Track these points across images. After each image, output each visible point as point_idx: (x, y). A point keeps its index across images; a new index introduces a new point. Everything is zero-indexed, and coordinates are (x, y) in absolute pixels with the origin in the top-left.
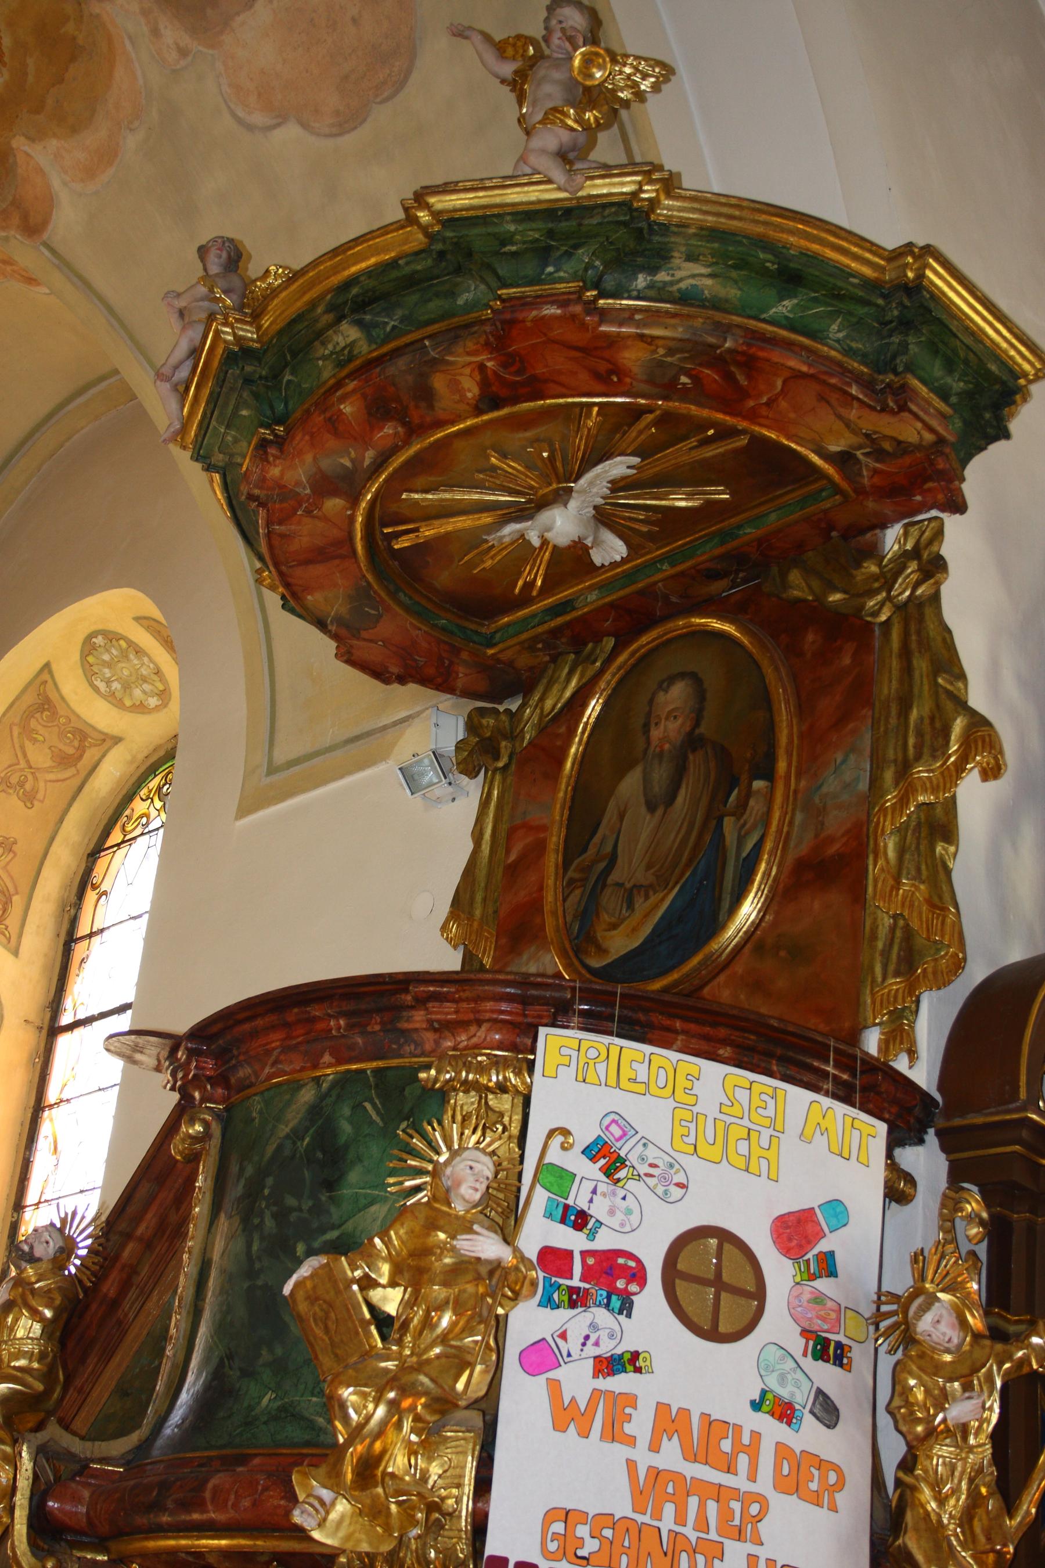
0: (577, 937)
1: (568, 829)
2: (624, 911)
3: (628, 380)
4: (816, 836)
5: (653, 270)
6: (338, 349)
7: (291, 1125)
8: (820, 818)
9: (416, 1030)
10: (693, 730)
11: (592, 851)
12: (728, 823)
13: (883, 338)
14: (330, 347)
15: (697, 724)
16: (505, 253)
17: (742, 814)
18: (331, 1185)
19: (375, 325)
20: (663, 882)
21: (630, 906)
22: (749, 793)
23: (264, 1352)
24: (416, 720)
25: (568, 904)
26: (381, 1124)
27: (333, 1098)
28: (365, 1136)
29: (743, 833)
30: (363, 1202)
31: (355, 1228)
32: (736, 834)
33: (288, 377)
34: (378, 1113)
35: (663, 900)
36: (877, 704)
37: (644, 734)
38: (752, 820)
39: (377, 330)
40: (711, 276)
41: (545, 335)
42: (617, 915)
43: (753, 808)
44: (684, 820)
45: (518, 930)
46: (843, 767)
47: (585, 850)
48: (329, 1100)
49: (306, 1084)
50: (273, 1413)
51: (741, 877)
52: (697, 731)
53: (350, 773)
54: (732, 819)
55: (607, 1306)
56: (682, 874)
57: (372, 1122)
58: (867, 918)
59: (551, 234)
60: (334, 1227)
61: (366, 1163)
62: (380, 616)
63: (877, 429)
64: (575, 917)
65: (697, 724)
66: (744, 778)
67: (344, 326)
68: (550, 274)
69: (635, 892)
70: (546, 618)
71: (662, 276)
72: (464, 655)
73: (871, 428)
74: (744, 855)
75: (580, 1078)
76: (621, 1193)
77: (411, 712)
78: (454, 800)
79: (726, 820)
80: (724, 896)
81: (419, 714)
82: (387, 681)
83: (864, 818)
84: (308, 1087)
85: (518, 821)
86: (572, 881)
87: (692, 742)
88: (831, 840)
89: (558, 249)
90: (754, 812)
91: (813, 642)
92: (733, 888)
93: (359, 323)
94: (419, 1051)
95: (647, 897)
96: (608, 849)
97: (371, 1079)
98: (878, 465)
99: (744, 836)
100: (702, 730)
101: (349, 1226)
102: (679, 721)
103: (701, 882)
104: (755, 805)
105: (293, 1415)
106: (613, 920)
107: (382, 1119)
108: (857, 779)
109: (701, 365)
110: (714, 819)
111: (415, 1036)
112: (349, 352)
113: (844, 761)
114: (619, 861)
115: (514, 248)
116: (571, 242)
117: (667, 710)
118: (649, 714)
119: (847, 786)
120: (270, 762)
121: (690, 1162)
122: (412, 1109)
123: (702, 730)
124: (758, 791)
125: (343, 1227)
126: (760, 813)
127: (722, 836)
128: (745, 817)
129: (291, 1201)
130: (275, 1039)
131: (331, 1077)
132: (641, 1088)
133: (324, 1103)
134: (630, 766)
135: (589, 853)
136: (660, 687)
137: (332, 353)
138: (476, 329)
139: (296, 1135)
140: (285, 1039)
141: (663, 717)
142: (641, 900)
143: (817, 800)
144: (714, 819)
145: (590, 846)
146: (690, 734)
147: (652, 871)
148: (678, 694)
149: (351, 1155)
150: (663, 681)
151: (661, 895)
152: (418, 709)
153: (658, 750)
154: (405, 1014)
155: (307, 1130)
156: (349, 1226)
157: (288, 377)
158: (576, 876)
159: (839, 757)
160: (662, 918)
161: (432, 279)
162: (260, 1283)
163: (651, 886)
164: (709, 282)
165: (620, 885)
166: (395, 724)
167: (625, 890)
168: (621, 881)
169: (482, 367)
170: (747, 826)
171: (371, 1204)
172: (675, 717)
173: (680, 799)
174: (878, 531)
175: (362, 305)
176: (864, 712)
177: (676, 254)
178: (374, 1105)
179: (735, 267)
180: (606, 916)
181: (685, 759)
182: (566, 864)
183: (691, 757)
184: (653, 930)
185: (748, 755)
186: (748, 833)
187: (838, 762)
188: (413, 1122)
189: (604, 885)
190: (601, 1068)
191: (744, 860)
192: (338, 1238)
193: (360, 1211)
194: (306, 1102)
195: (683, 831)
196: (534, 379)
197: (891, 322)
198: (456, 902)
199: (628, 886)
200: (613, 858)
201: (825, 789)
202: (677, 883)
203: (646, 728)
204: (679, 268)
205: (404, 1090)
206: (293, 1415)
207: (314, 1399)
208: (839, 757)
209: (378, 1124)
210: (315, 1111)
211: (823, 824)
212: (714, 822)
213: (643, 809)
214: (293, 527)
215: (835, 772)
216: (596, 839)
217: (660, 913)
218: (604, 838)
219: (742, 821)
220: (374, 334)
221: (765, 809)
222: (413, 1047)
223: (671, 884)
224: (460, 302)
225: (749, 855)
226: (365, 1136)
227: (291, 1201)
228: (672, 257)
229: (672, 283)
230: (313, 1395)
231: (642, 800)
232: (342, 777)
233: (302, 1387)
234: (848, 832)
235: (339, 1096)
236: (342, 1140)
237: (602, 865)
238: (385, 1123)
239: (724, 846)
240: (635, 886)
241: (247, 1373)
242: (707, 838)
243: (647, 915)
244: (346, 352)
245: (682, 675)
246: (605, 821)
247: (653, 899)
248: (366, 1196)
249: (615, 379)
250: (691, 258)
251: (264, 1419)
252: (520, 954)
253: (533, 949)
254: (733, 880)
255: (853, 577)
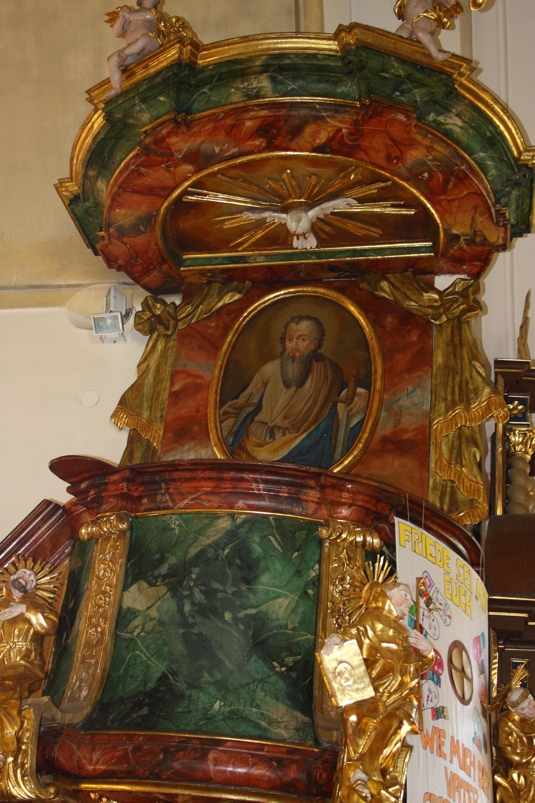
0: (232, 445)
2: (268, 438)
3: (400, 165)
4: (395, 426)
5: (439, 114)
6: (250, 87)
7: (212, 539)
8: (398, 418)
9: (307, 501)
10: (316, 349)
11: (242, 399)
12: (341, 407)
13: (503, 187)
14: (246, 84)
16: (381, 76)
17: (350, 404)
18: (249, 581)
19: (282, 83)
20: (296, 428)
22: (354, 394)
23: (206, 675)
24: (85, 288)
25: (224, 424)
26: (281, 551)
28: (271, 556)
29: (350, 414)
30: (272, 595)
31: (268, 610)
32: (346, 414)
33: (205, 90)
34: (279, 544)
35: (296, 438)
36: (434, 366)
37: (281, 343)
38: (356, 409)
39: (282, 86)
40: (461, 128)
41: (386, 127)
42: (263, 439)
43: (357, 402)
47: (237, 397)
49: (224, 517)
50: (227, 715)
51: (349, 438)
52: (319, 351)
53: (32, 306)
54: (344, 405)
55: (433, 679)
56: (309, 427)
57: (275, 549)
59: (409, 77)
60: (252, 607)
61: (273, 572)
62: (144, 232)
63: (483, 230)
64: (230, 433)
65: (319, 346)
66: (351, 384)
67: (264, 76)
68: (397, 96)
69: (275, 429)
71: (441, 119)
72: (165, 267)
73: (481, 229)
74: (352, 426)
78: (115, 342)
79: (339, 405)
80: (338, 445)
81: (88, 285)
82: (110, 266)
83: (428, 425)
84: (225, 519)
85: (180, 368)
86: (226, 413)
87: (315, 355)
88: (405, 431)
89: (407, 84)
90: (358, 405)
91: (391, 323)
92: (344, 442)
93: (273, 79)
95: (284, 434)
96: (256, 400)
98: (465, 246)
99: (351, 416)
100: (322, 351)
101: (263, 608)
102: (307, 343)
103: (322, 434)
104: (359, 402)
105: (242, 718)
106: (259, 441)
107: (282, 548)
108: (422, 403)
109: (440, 171)
110: (331, 402)
111: (304, 504)
112: (257, 92)
113: (413, 391)
114: (264, 410)
115: (387, 75)
116: (415, 85)
117: (298, 334)
118: (285, 333)
119: (415, 405)
121: (450, 603)
122: (300, 546)
123: (322, 351)
124: (360, 394)
125: (260, 607)
126: (361, 406)
127: (336, 413)
128: (351, 406)
130: (207, 486)
131: (243, 516)
133: (239, 531)
134: (272, 358)
135: (239, 400)
137: (244, 88)
138: (348, 109)
139: (217, 546)
140: (215, 487)
141: (295, 337)
142: (281, 435)
144: (331, 402)
145: (241, 396)
146: (314, 352)
147: (288, 420)
148: (305, 327)
149: (262, 565)
150: (294, 318)
151: (295, 435)
153: (291, 354)
154: (304, 490)
155: (226, 545)
157: (205, 90)
158: (230, 410)
159: (410, 389)
160: (295, 448)
161: (331, 72)
162: (195, 631)
163: (287, 429)
164: (458, 130)
165: (263, 423)
166: (68, 286)
167: (268, 427)
169: (340, 130)
170: (353, 411)
171: (278, 597)
172: (303, 340)
173: (308, 384)
175: (282, 69)
176: (427, 368)
177: (454, 110)
178: (276, 539)
179: (474, 128)
181: (311, 364)
182: (222, 403)
183: (315, 364)
184: (289, 453)
185: (354, 373)
186: (354, 415)
189: (252, 421)
191: (351, 428)
192: (256, 614)
193: (270, 600)
194: (223, 528)
195: (309, 404)
196: (359, 148)
197: (512, 180)
198: (123, 402)
199: (271, 425)
200: (259, 408)
201: (400, 403)
202: (305, 431)
203: (283, 340)
204: (451, 118)
206: (242, 718)
207: (254, 710)
210: (231, 535)
211: (400, 421)
212: (331, 404)
213: (281, 385)
214: (151, 172)
217: (294, 445)
219: (350, 408)
220: (279, 88)
221: (365, 405)
222: (301, 510)
223: (300, 432)
224: (339, 90)
226: (271, 556)
227: (216, 585)
228: (451, 111)
229: (443, 124)
230: (252, 707)
231: (280, 379)
233: (243, 701)
234: (416, 429)
235: (250, 529)
236: (255, 555)
237: (250, 409)
238: (284, 551)
239: (338, 418)
240: (275, 426)
241: (194, 685)
242: (327, 411)
244: (255, 91)
245: (309, 318)
246: (252, 386)
247: (288, 436)
248: (274, 592)
249: (395, 162)
250: (458, 116)
251: (221, 717)
252: (182, 445)
253: (192, 444)
254: (344, 438)
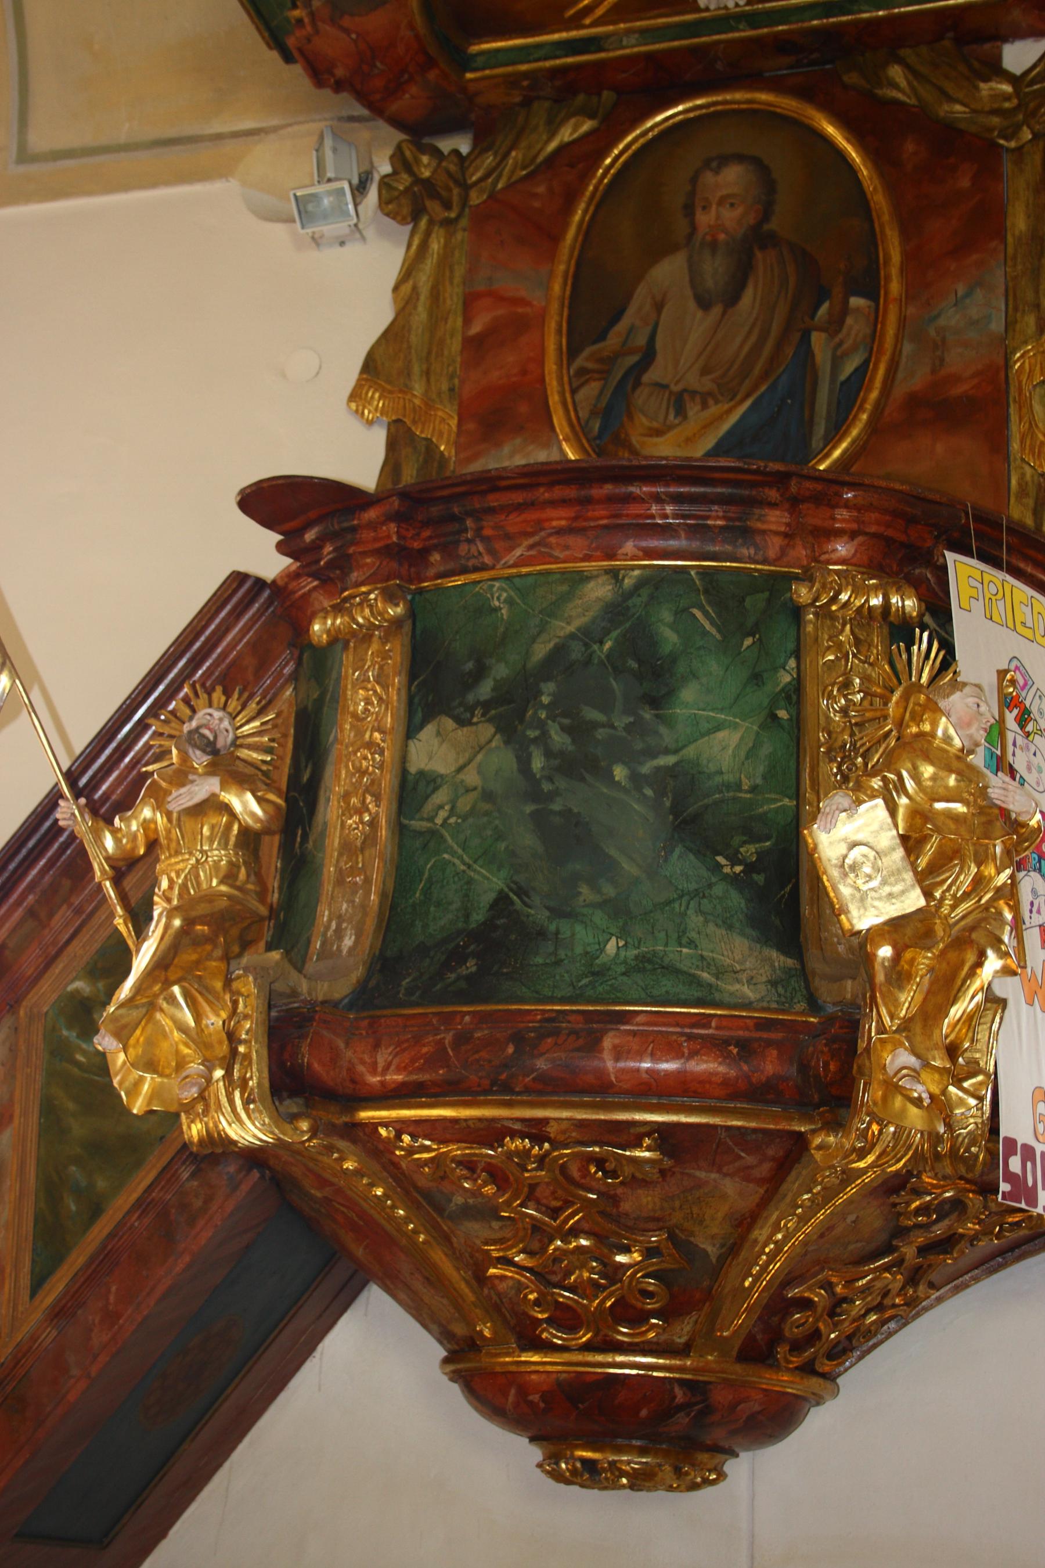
0: (599, 437)
1: (570, 308)
2: (671, 416)
4: (933, 372)
7: (577, 623)
8: (939, 353)
9: (764, 532)
11: (613, 340)
12: (818, 340)
15: (766, 214)
17: (837, 332)
18: (655, 702)
20: (728, 390)
21: (681, 411)
24: (272, 136)
26: (718, 637)
27: (644, 598)
28: (699, 648)
29: (839, 353)
30: (705, 726)
34: (713, 623)
35: (729, 411)
44: (754, 325)
45: (494, 415)
46: (968, 301)
47: (602, 337)
48: (636, 600)
49: (597, 576)
51: (839, 402)
52: (766, 227)
54: (824, 335)
57: (705, 633)
58: (1013, 473)
60: (667, 751)
61: (704, 680)
64: (593, 413)
65: (766, 214)
69: (686, 396)
70: (558, 53)
72: (432, 75)
74: (843, 377)
75: (988, 616)
76: (1033, 749)
77: (264, 125)
81: (275, 129)
84: (600, 580)
86: (582, 372)
87: (757, 238)
92: (828, 412)
94: (759, 557)
95: (705, 406)
96: (641, 340)
97: (697, 582)
100: (773, 225)
101: (690, 752)
102: (740, 210)
104: (855, 327)
106: (655, 425)
107: (719, 631)
113: (968, 294)
114: (659, 358)
118: (692, 194)
120: (22, 146)
123: (773, 225)
124: (858, 310)
125: (684, 752)
127: (809, 354)
128: (840, 336)
129: (592, 714)
130: (559, 518)
132: (1028, 633)
133: (630, 603)
134: (667, 249)
136: (707, 164)
139: (588, 636)
142: (698, 407)
143: (932, 333)
148: (733, 178)
149: (681, 668)
151: (726, 407)
152: (275, 122)
153: (708, 238)
154: (757, 511)
155: (607, 632)
156: (690, 752)
158: (590, 365)
159: (961, 289)
162: (556, 806)
163: (710, 394)
166: (235, 135)
167: (671, 393)
168: (664, 382)
170: (845, 346)
174: (999, 43)
178: (706, 614)
180: (644, 420)
182: (573, 352)
183: (759, 255)
187: (960, 294)
188: (760, 639)
189: (637, 383)
190: (1001, 604)
191: (843, 384)
192: (676, 764)
193: (703, 735)
194: (598, 599)
200: (648, 356)
201: (942, 322)
203: (689, 210)
205: (744, 601)
207: (685, 950)
208: (961, 289)
209: (714, 637)
210: (615, 612)
211: (942, 360)
213: (692, 304)
215: (955, 305)
216: (622, 326)
218: (631, 330)
219: (837, 340)
222: (752, 551)
223: (739, 397)
225: (849, 378)
226: (699, 648)
227: (592, 714)
230: (681, 945)
231: (689, 292)
232: (154, 185)
233: (662, 935)
235: (652, 597)
236: (667, 649)
237: (632, 360)
239: (814, 364)
240: (685, 390)
242: (789, 351)
243: (706, 426)
245: (740, 158)
246: (631, 310)
247: (714, 410)
248: (708, 719)
254: (829, 404)
255: (977, 88)
